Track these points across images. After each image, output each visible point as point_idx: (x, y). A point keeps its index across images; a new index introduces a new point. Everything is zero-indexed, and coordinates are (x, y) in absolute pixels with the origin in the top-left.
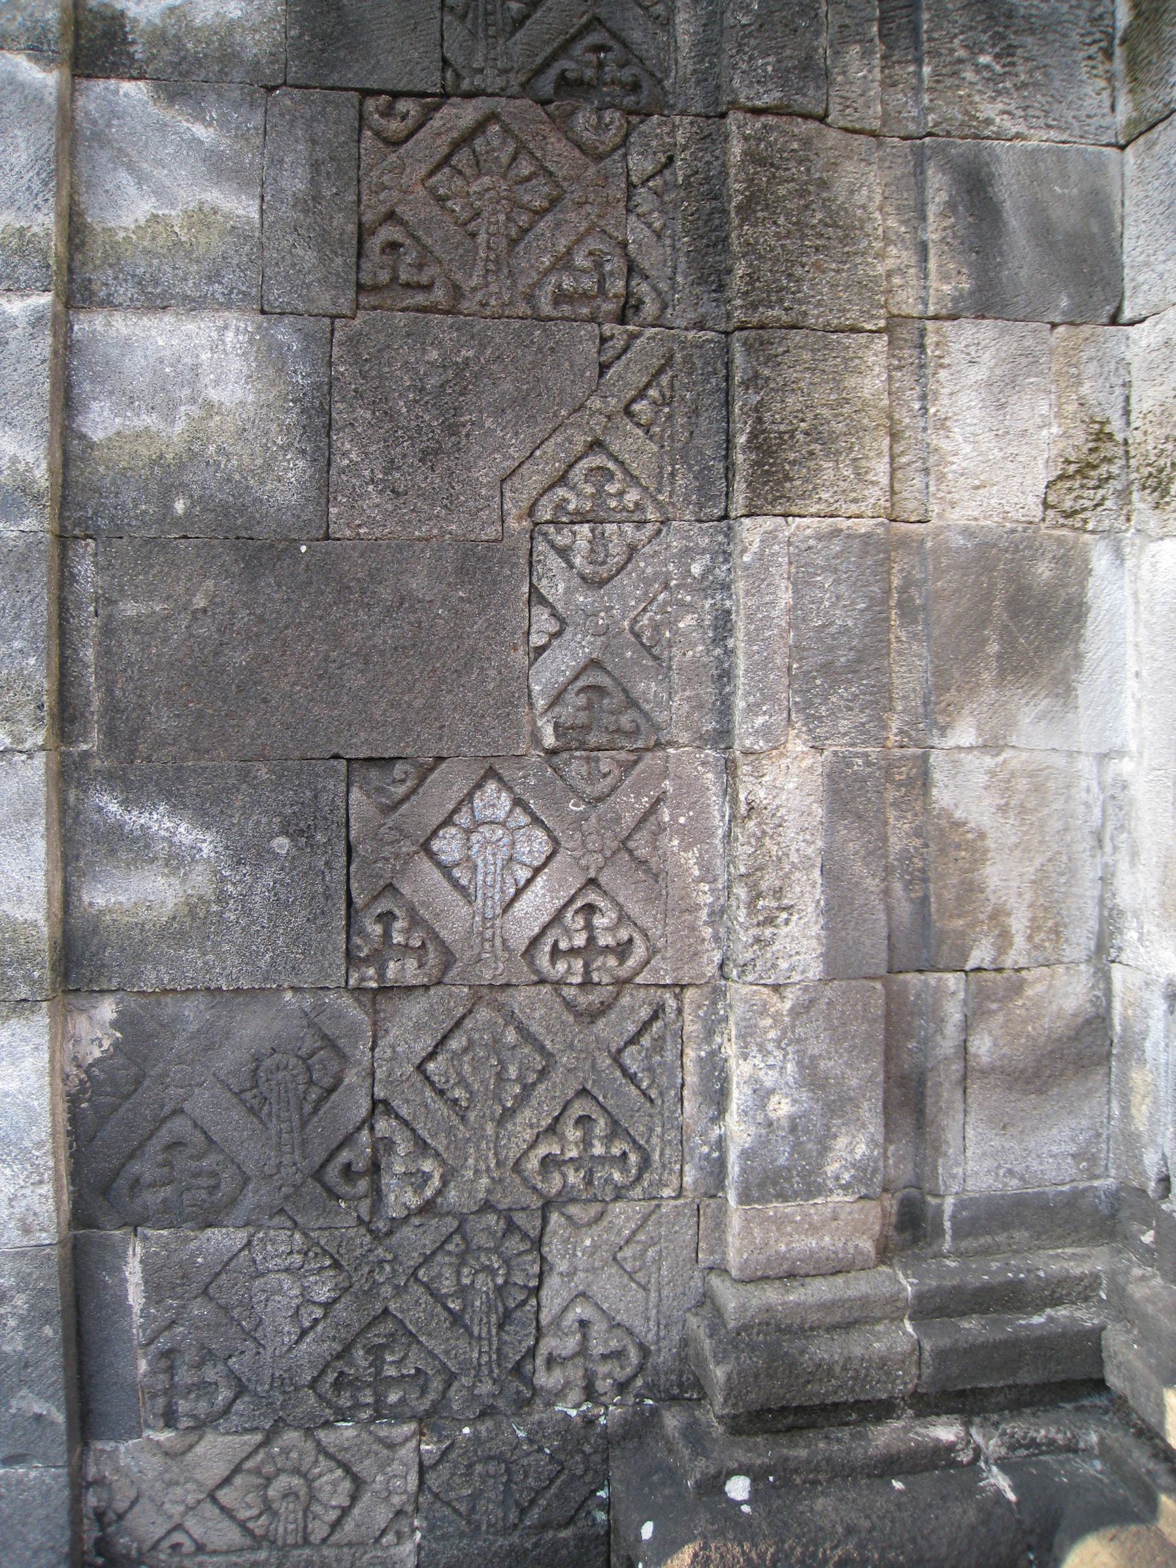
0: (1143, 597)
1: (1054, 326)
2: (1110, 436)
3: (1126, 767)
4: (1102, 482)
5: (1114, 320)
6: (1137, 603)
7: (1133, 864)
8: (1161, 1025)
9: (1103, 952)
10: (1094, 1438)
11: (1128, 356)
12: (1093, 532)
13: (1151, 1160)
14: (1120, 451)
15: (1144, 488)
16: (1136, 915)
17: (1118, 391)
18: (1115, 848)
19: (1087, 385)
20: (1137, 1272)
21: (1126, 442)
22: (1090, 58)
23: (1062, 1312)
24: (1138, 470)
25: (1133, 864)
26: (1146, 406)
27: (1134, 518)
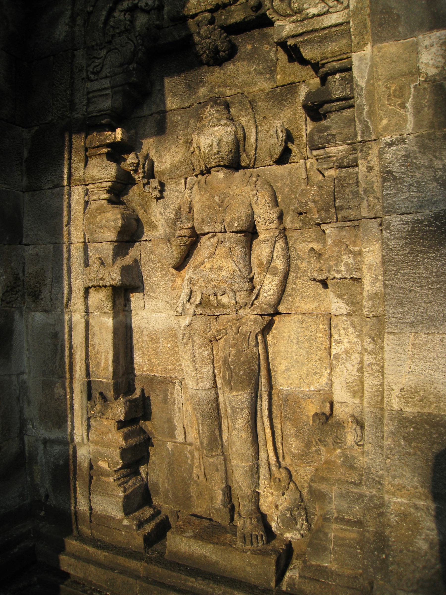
0: (30, 327)
1: (5, 245)
2: (19, 279)
3: (25, 377)
4: (17, 292)
5: (20, 243)
6: (27, 328)
7: (29, 405)
8: (42, 452)
9: (22, 432)
10: (35, 579)
11: (24, 255)
12: (15, 308)
13: (42, 491)
14: (22, 283)
15: (29, 295)
16: (31, 420)
17: (21, 265)
18: (23, 401)
19: (13, 263)
20: (41, 525)
21: (23, 280)
22: (17, 165)
23: (22, 545)
24: (27, 289)
25: (29, 405)
26: (30, 271)
27: (26, 303)
